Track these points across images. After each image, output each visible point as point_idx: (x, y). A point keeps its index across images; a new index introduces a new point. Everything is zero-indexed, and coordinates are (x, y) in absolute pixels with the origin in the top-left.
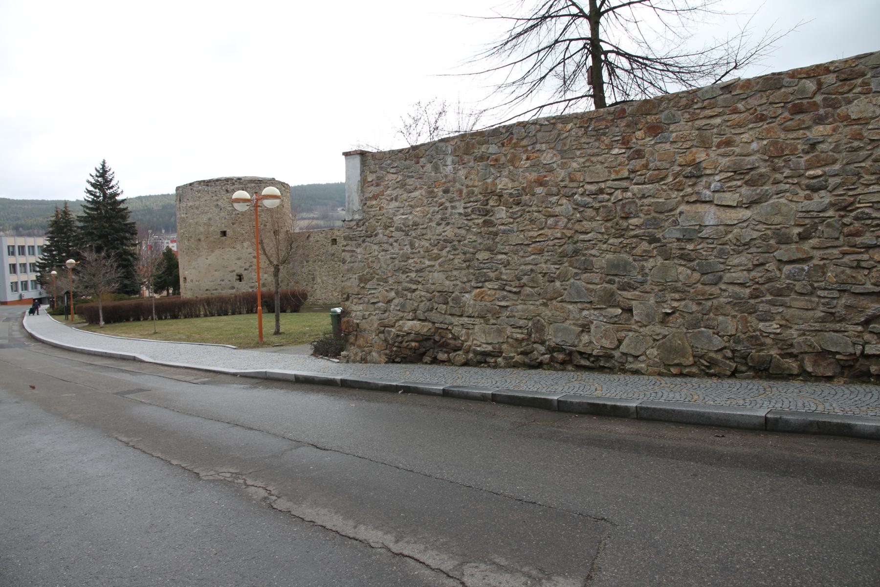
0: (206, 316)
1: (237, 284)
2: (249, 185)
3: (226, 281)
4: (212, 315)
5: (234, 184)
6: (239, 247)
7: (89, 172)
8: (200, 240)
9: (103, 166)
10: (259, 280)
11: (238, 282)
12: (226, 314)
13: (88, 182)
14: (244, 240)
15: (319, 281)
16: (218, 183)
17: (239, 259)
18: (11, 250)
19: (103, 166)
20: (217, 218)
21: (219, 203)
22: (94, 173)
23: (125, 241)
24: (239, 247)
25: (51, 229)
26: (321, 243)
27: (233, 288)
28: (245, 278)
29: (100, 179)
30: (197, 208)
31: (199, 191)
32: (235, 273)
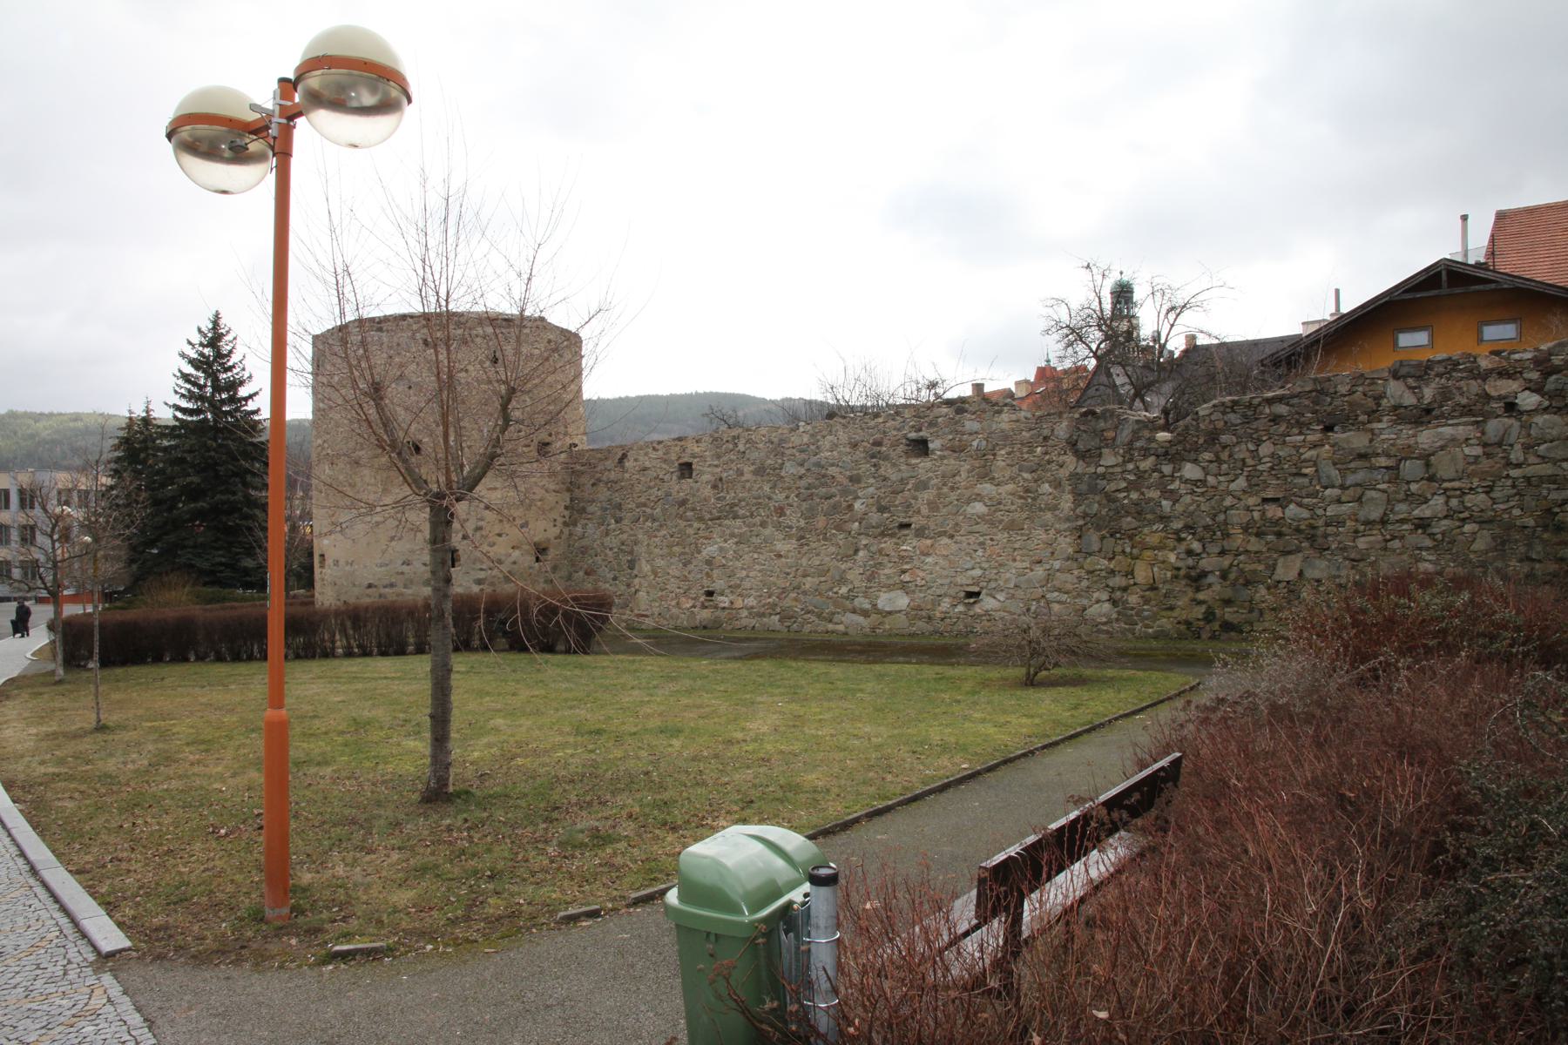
0: (349, 654)
4: (365, 653)
7: (184, 337)
12: (401, 651)
13: (183, 355)
15: (646, 568)
22: (196, 339)
23: (249, 478)
26: (652, 473)
29: (207, 351)
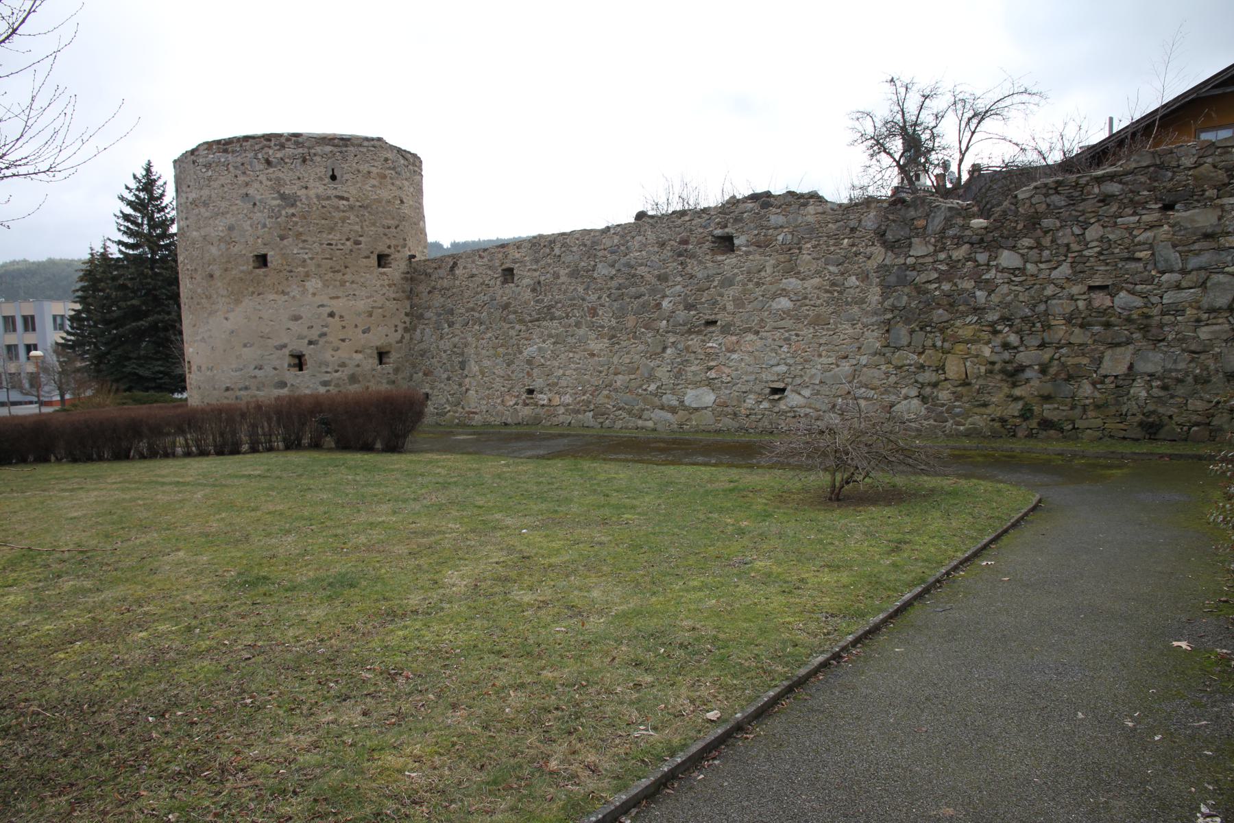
1: (292, 376)
2: (318, 149)
3: (268, 369)
4: (203, 453)
5: (283, 146)
6: (295, 291)
8: (211, 276)
9: (148, 170)
10: (343, 367)
11: (295, 371)
12: (235, 451)
13: (122, 199)
14: (307, 275)
15: (475, 369)
16: (247, 144)
17: (296, 318)
18: (59, 321)
19: (148, 170)
20: (246, 225)
21: (251, 191)
24: (295, 291)
25: (82, 284)
27: (283, 384)
28: (309, 362)
29: (142, 195)
30: (205, 204)
31: (208, 166)
32: (286, 351)
